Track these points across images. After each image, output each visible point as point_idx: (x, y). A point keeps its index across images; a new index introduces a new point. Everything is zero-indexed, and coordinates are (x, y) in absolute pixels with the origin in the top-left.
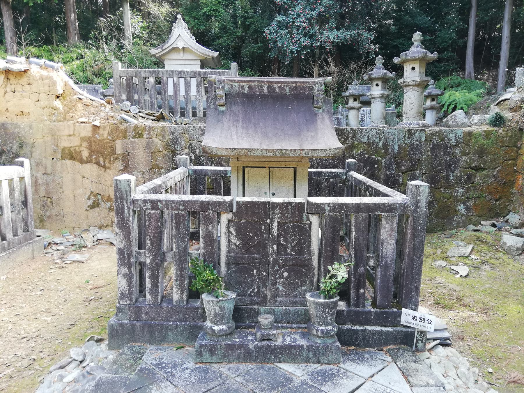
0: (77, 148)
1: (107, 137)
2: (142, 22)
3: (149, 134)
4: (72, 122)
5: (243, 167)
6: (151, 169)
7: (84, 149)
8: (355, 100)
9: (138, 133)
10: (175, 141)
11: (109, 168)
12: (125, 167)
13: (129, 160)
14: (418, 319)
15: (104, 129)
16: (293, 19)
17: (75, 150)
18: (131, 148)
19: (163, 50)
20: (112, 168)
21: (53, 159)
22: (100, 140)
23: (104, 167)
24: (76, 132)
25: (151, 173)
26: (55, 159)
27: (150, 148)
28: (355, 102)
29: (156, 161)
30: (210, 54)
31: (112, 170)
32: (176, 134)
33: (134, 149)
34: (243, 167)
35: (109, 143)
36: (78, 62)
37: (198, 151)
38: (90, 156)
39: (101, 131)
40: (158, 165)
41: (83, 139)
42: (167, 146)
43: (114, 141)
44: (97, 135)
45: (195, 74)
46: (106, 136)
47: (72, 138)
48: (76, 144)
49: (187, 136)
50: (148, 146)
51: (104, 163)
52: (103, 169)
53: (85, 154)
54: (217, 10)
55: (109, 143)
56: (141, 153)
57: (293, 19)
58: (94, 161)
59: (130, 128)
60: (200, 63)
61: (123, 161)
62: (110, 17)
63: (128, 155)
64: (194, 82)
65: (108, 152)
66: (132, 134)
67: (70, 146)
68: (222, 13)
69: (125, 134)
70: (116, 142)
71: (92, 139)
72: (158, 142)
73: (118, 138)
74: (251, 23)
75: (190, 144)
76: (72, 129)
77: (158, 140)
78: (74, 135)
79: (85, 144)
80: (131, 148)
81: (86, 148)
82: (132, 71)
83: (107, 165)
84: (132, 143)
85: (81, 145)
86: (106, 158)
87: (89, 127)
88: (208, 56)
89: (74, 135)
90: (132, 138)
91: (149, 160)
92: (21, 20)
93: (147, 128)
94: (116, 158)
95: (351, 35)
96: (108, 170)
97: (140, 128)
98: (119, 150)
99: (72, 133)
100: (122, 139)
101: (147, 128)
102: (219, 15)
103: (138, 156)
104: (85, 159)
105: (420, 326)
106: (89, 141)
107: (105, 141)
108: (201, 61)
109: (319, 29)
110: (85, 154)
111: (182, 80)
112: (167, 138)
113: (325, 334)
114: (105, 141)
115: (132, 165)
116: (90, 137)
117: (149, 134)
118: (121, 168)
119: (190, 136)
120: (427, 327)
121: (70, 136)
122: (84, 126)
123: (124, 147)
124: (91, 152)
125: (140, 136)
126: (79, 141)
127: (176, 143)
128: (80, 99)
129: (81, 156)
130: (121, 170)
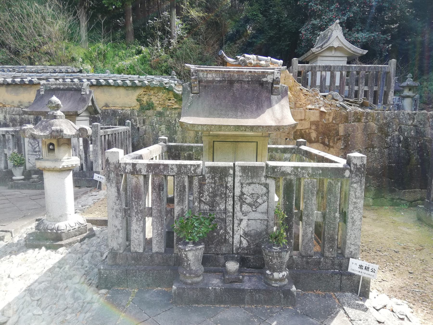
0: (307, 131)
1: (332, 121)
2: (182, 24)
3: (366, 119)
4: (302, 109)
5: (214, 141)
6: (367, 148)
7: (313, 131)
8: (410, 90)
9: (358, 118)
10: (388, 125)
11: (333, 147)
12: (346, 147)
13: (349, 141)
14: (364, 268)
15: (329, 115)
16: (326, 22)
17: (305, 132)
18: (351, 131)
19: (323, 48)
20: (335, 147)
21: (286, 139)
22: (326, 124)
23: (328, 146)
24: (306, 117)
25: (367, 152)
26: (288, 139)
27: (367, 130)
28: (410, 92)
29: (372, 141)
30: (361, 52)
31: (335, 149)
32: (389, 119)
33: (353, 131)
34: (214, 141)
35: (334, 126)
36: (137, 57)
37: (406, 133)
38: (318, 137)
39: (327, 117)
40: (373, 145)
41: (312, 123)
42: (381, 129)
43: (338, 124)
44: (323, 120)
45: (341, 69)
46: (331, 120)
47: (303, 122)
48: (306, 127)
49: (398, 121)
50: (366, 128)
51: (329, 143)
52: (328, 148)
53: (314, 135)
54: (256, 15)
55: (334, 126)
56: (359, 135)
57: (326, 22)
58: (320, 141)
59: (351, 114)
60: (346, 59)
61: (345, 141)
62: (156, 20)
63: (349, 136)
64: (338, 74)
65: (333, 133)
66: (352, 119)
67: (302, 128)
68: (260, 17)
69: (346, 119)
70: (340, 125)
71: (320, 123)
72: (373, 125)
73: (341, 122)
74: (285, 25)
75: (400, 127)
76: (303, 115)
77: (374, 124)
78: (305, 119)
79: (313, 127)
80: (351, 131)
81: (314, 130)
82: (309, 66)
83: (331, 144)
84: (353, 126)
85: (310, 128)
86: (330, 139)
87: (317, 114)
88: (357, 53)
89: (305, 119)
90: (353, 122)
91: (365, 140)
92: (103, 22)
93: (365, 113)
94: (339, 139)
95: (374, 36)
96: (332, 149)
97: (359, 114)
98: (341, 133)
99: (303, 118)
100: (344, 123)
101: (365, 113)
102: (258, 19)
103: (357, 137)
104: (313, 139)
105: (359, 272)
106: (315, 124)
107: (330, 125)
108: (348, 58)
109: (348, 31)
110: (314, 135)
111: (329, 73)
112: (382, 122)
113: (255, 281)
114: (330, 125)
115: (352, 145)
116: (318, 122)
117: (366, 119)
118: (342, 147)
119: (400, 121)
120: (371, 275)
121: (301, 120)
122: (313, 112)
123: (346, 130)
124: (319, 133)
125: (359, 120)
126: (309, 125)
127: (388, 126)
128: (301, 90)
129: (310, 137)
130: (342, 149)
